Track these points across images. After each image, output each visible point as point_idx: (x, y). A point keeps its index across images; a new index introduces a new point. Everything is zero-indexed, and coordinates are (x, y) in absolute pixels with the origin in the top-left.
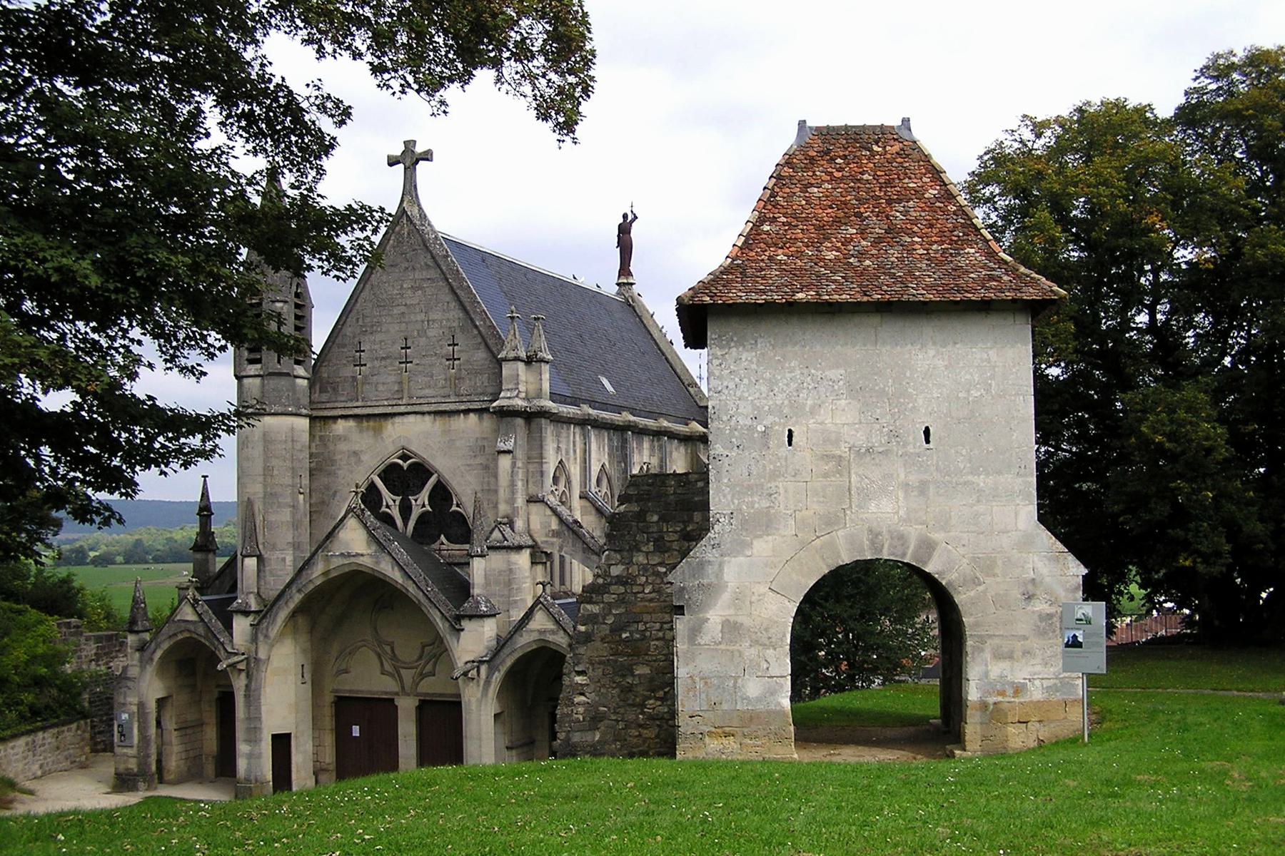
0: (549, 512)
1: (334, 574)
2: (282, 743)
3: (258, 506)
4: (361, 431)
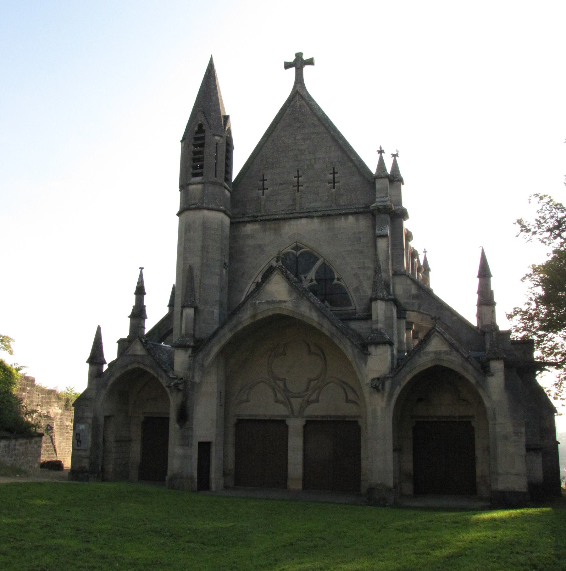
0: (409, 282)
1: (260, 317)
2: (205, 448)
3: (197, 272)
4: (265, 231)
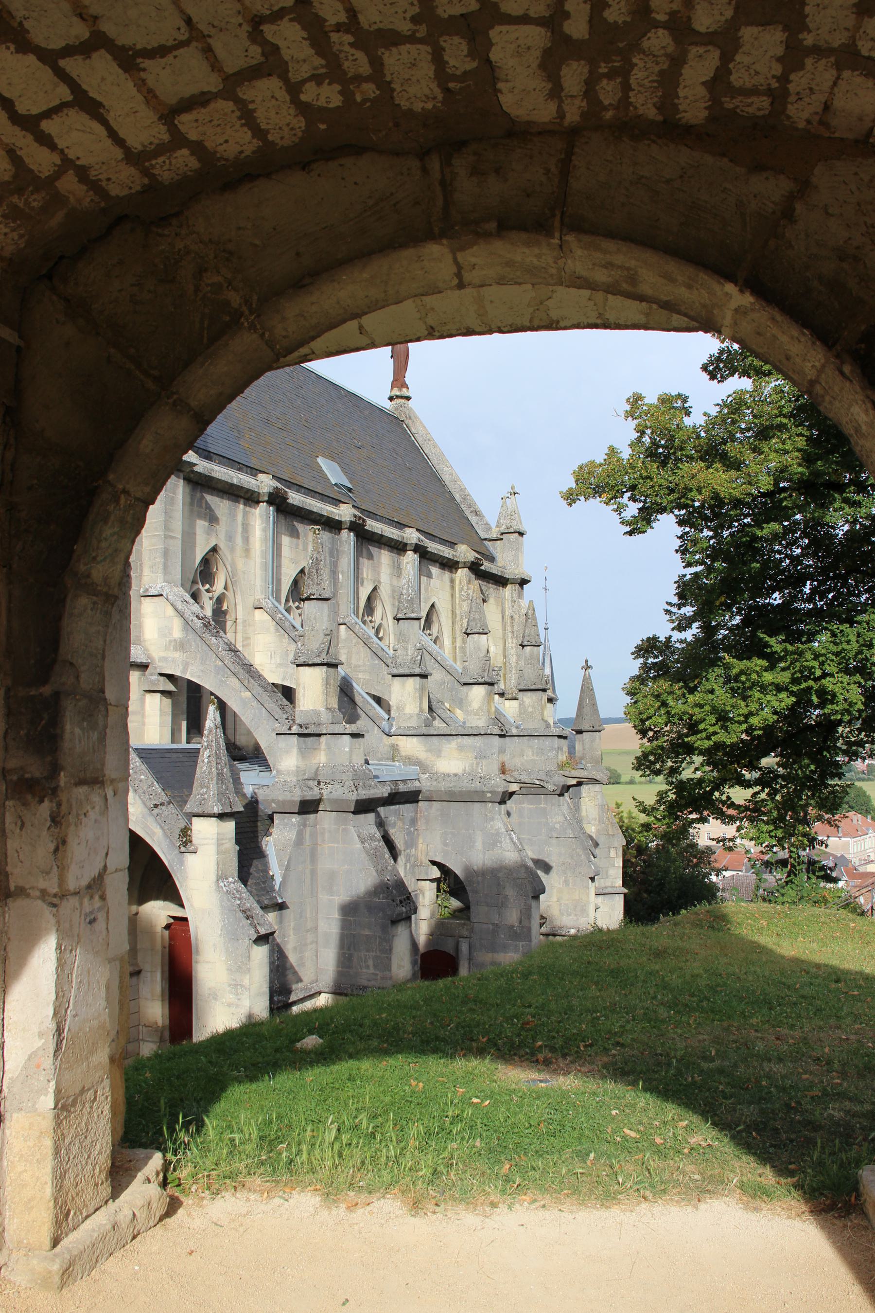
0: (170, 611)
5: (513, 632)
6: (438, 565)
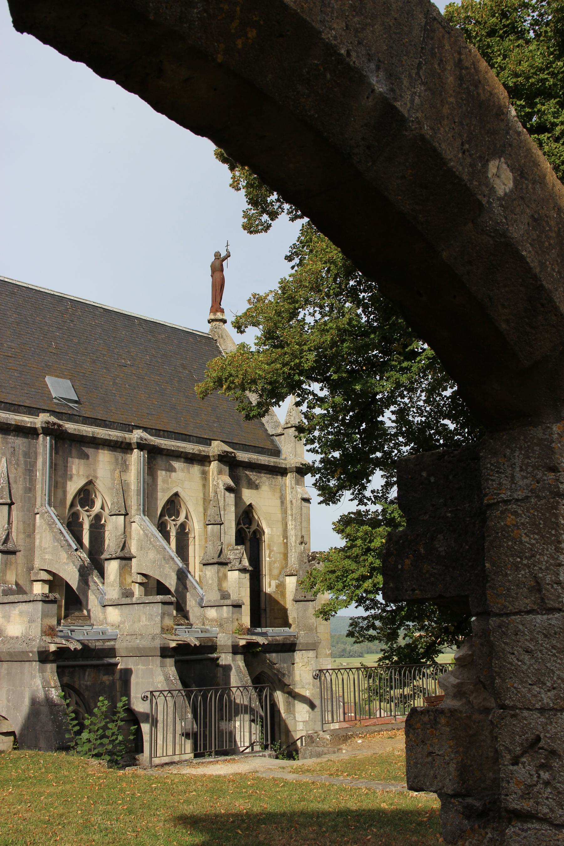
5: (292, 515)
6: (183, 460)
